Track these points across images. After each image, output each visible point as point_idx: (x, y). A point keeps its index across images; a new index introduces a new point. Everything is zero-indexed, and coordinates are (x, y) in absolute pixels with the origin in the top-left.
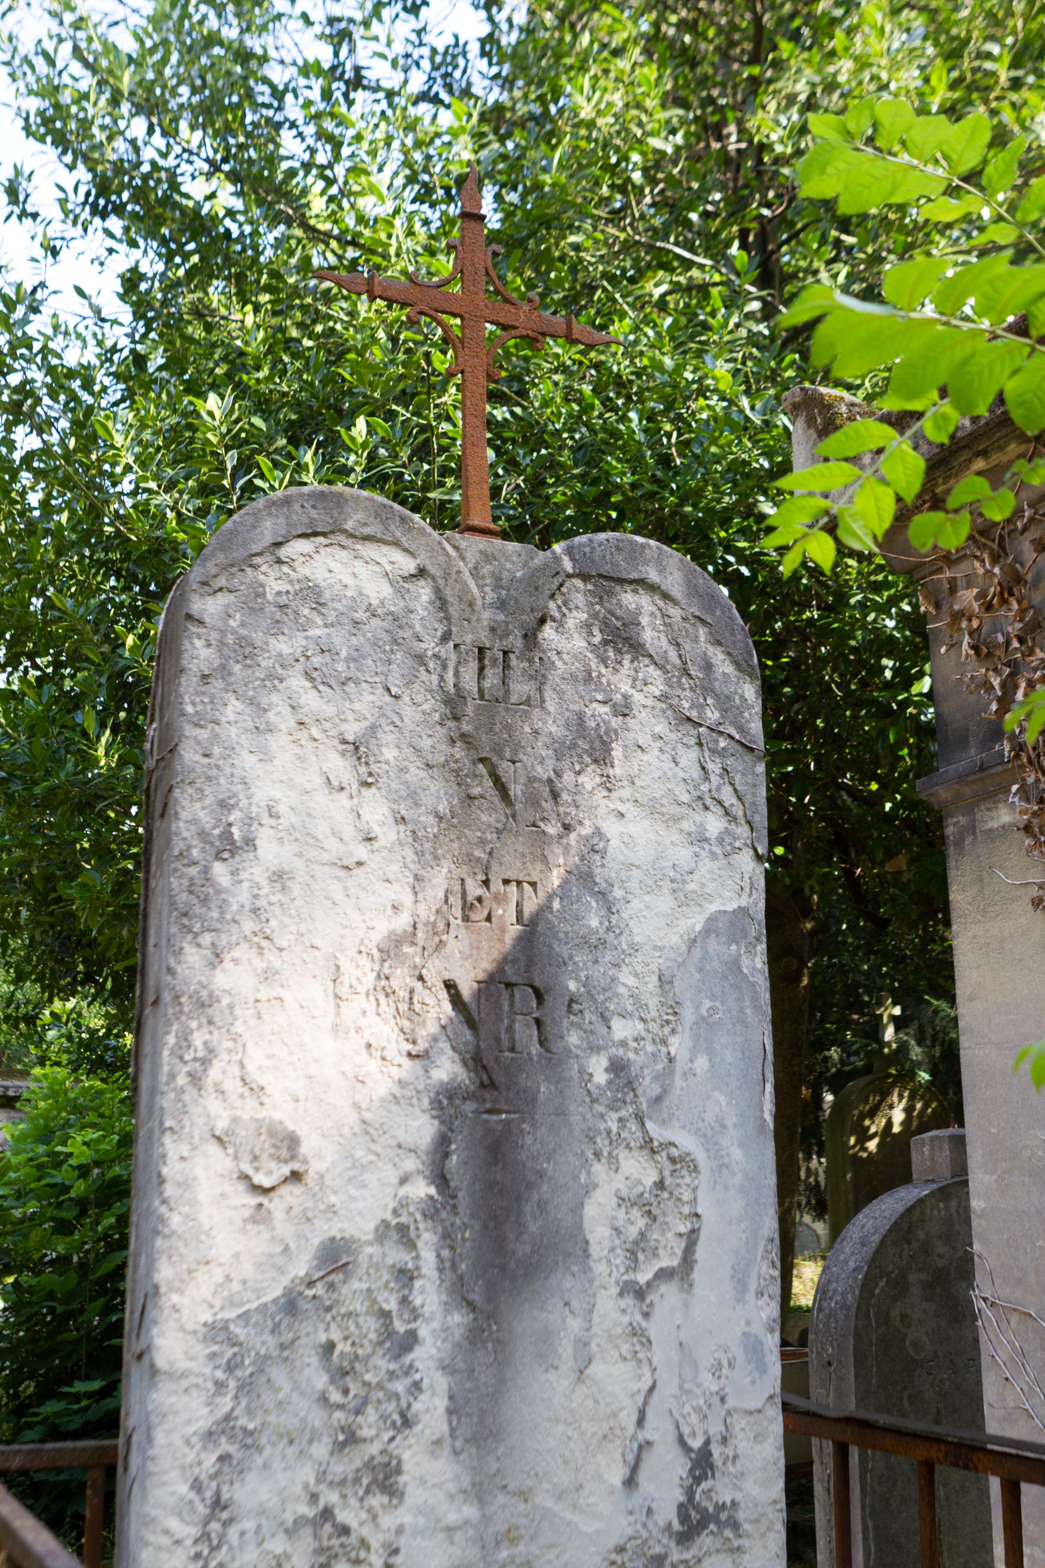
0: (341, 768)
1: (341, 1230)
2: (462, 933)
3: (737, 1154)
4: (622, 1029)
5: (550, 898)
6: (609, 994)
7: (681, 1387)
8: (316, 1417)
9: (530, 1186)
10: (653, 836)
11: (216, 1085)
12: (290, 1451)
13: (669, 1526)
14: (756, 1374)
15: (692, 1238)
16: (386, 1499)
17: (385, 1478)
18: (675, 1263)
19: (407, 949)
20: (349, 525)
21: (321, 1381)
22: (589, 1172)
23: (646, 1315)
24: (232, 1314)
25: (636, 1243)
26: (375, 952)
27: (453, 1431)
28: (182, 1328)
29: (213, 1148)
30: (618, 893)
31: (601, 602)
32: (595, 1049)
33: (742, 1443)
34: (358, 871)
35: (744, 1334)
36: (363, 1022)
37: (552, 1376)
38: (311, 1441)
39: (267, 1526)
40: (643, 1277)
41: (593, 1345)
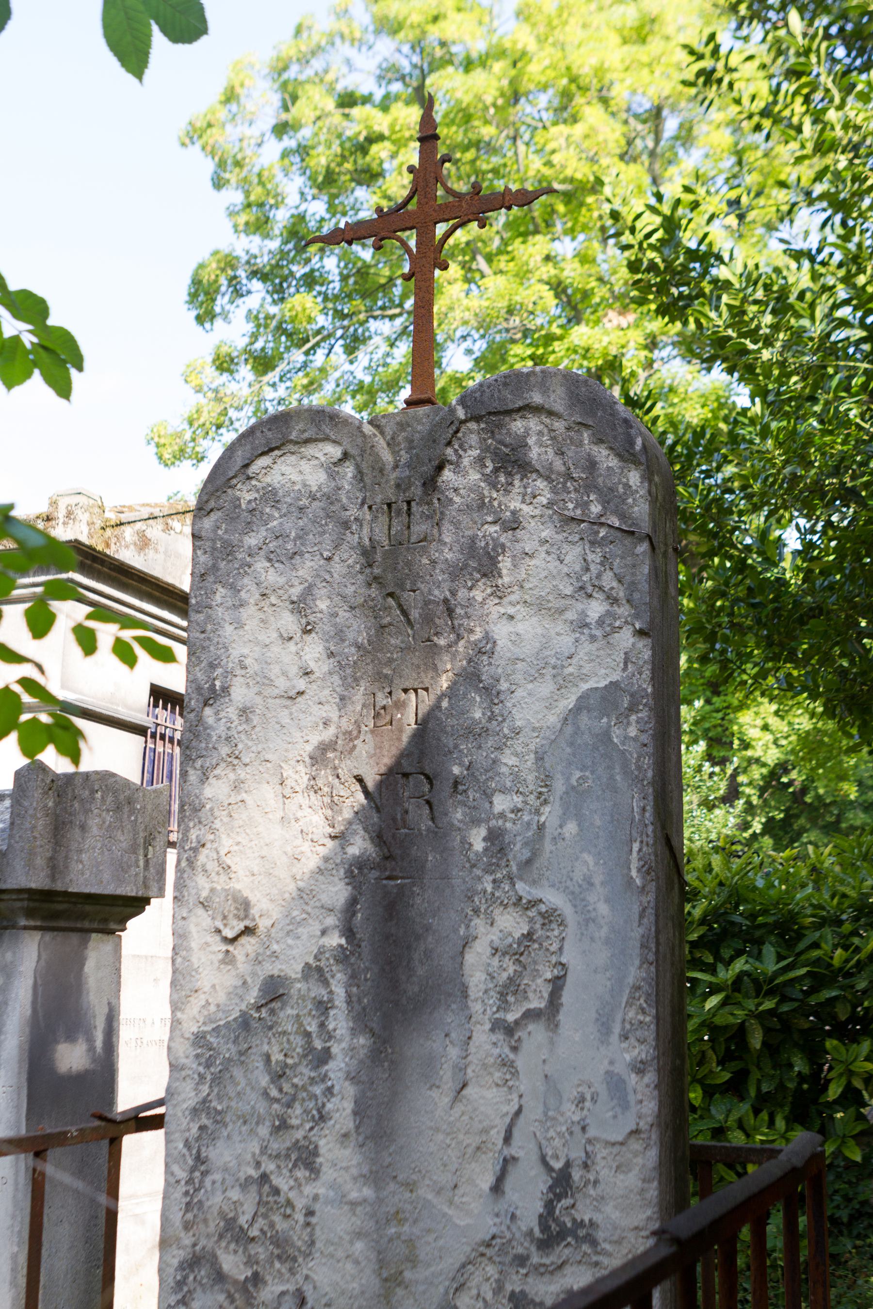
0: (289, 622)
1: (281, 970)
2: (369, 737)
3: (603, 909)
4: (501, 803)
5: (440, 699)
6: (490, 774)
7: (545, 1114)
8: (262, 1107)
9: (418, 938)
10: (539, 631)
11: (203, 866)
12: (244, 1128)
13: (530, 1232)
14: (618, 1110)
15: (557, 984)
16: (307, 1174)
17: (306, 1158)
18: (542, 1005)
19: (330, 755)
20: (293, 436)
21: (264, 1080)
22: (468, 927)
23: (515, 1049)
24: (208, 1028)
25: (505, 986)
26: (307, 759)
27: (357, 1128)
28: (182, 1036)
29: (200, 911)
30: (504, 686)
31: (493, 437)
32: (476, 822)
33: (603, 1169)
34: (299, 699)
35: (607, 1072)
36: (300, 814)
37: (434, 1094)
38: (257, 1123)
39: (230, 1180)
40: (511, 1017)
41: (469, 1071)
